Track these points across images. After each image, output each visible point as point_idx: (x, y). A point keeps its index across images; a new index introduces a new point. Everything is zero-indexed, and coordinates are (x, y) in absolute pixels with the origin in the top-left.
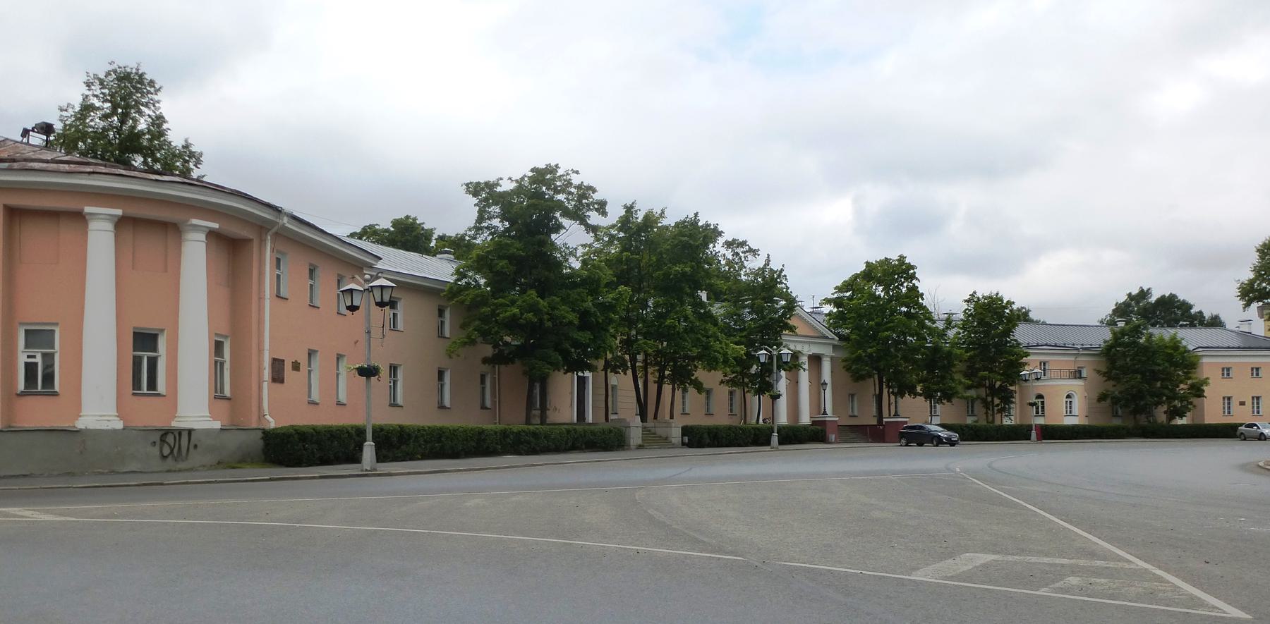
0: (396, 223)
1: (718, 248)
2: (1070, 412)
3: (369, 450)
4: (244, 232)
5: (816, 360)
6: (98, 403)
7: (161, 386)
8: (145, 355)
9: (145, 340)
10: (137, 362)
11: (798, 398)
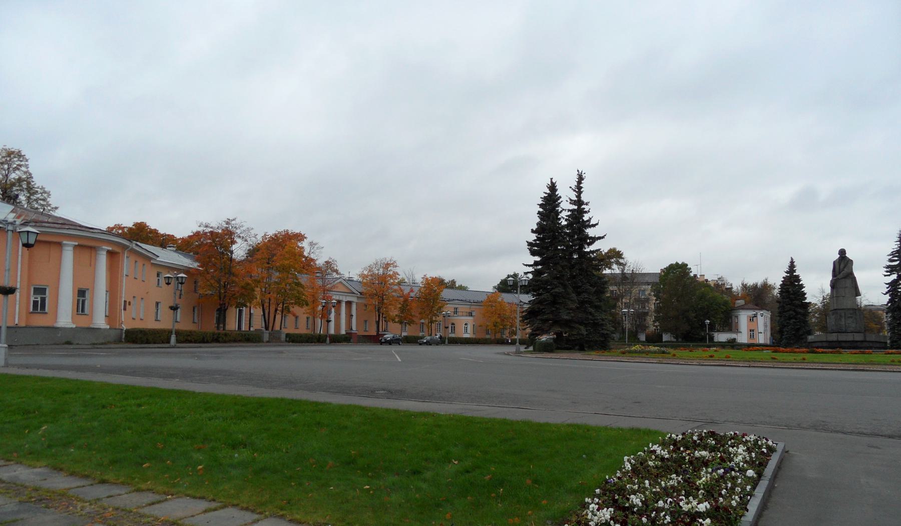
0: (136, 225)
1: (305, 244)
2: (466, 331)
3: (173, 339)
4: (117, 250)
5: (349, 304)
7: (86, 311)
8: (81, 299)
9: (81, 293)
10: (78, 301)
11: (338, 323)
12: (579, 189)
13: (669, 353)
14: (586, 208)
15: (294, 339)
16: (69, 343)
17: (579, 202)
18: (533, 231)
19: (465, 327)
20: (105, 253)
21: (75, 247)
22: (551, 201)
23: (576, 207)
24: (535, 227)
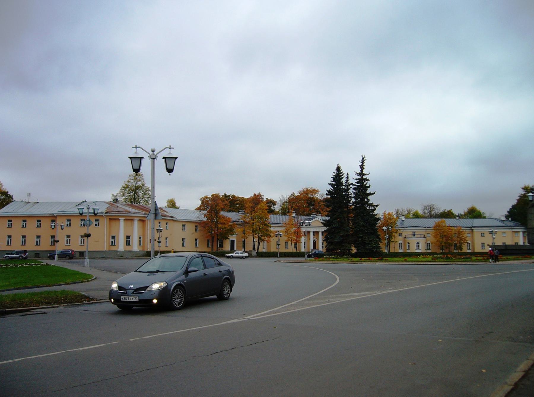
6: (121, 246)
9: (128, 237)
12: (362, 167)
15: (261, 255)
16: (122, 257)
17: (361, 174)
19: (418, 243)
23: (359, 177)
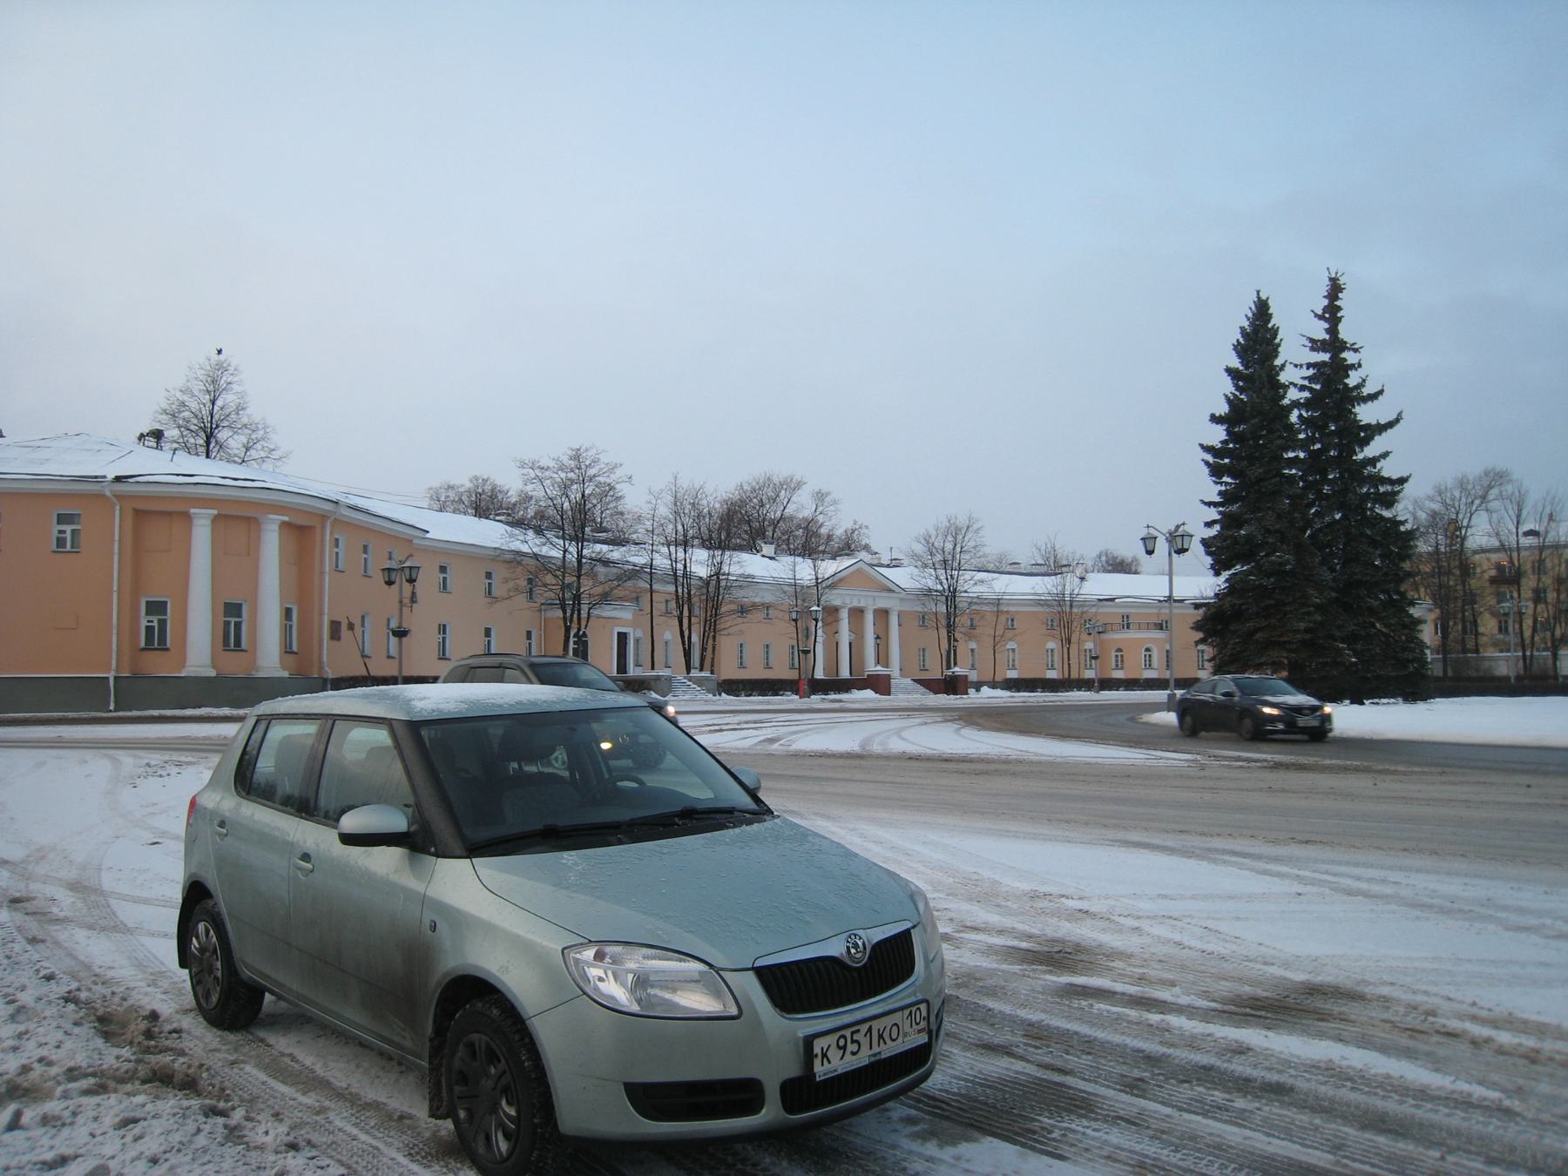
2: (1149, 666)
8: (233, 620)
9: (233, 609)
10: (227, 624)
12: (1332, 314)
13: (991, 950)
14: (1350, 357)
17: (1334, 344)
18: (1215, 419)
20: (276, 527)
21: (284, 525)
22: (1258, 340)
23: (1325, 357)
24: (1223, 409)
